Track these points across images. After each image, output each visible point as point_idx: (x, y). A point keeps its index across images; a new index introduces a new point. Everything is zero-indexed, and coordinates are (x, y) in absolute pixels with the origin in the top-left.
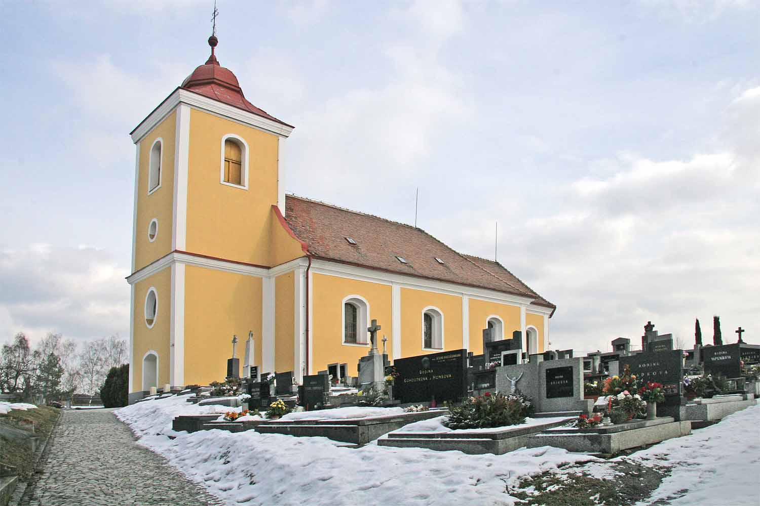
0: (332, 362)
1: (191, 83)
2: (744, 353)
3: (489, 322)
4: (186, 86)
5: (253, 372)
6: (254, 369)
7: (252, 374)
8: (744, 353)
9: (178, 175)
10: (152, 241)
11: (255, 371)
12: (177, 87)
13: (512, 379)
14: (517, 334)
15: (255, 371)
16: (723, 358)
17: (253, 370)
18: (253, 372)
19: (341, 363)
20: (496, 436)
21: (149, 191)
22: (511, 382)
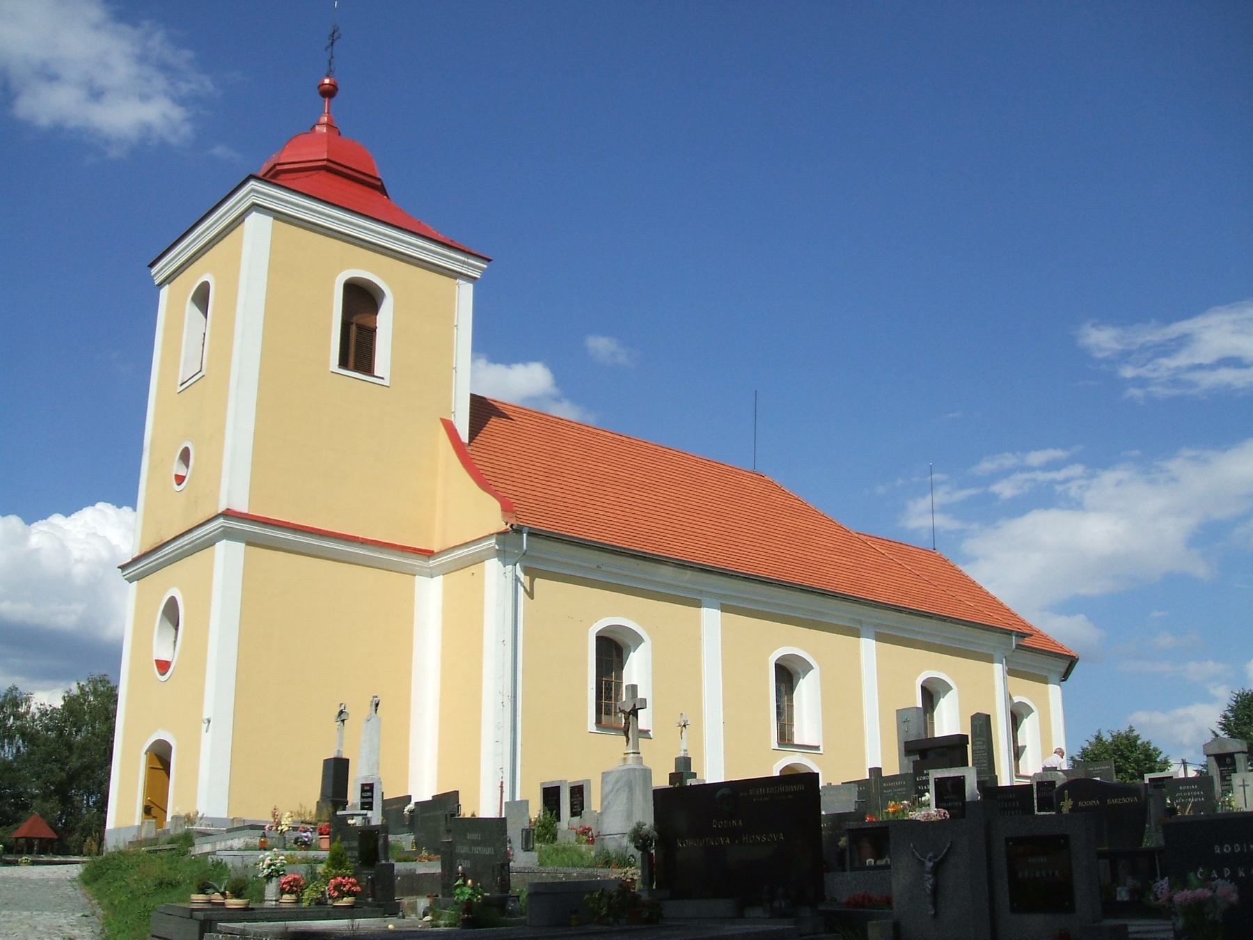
0: (551, 778)
1: (278, 168)
2: (1222, 846)
3: (924, 689)
4: (268, 176)
5: (365, 795)
6: (366, 788)
7: (370, 800)
8: (1222, 846)
9: (553, 782)
10: (178, 488)
11: (369, 794)
12: (248, 175)
13: (925, 858)
14: (982, 724)
15: (369, 794)
16: (1238, 850)
17: (367, 791)
18: (365, 795)
19: (574, 778)
20: (448, 917)
21: (180, 383)
22: (923, 863)
